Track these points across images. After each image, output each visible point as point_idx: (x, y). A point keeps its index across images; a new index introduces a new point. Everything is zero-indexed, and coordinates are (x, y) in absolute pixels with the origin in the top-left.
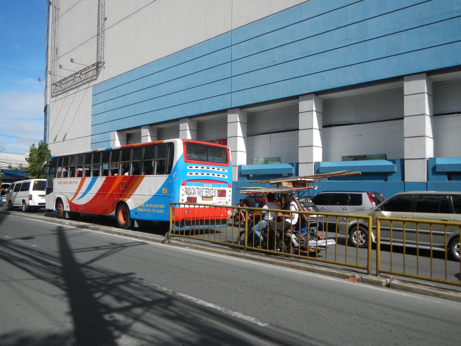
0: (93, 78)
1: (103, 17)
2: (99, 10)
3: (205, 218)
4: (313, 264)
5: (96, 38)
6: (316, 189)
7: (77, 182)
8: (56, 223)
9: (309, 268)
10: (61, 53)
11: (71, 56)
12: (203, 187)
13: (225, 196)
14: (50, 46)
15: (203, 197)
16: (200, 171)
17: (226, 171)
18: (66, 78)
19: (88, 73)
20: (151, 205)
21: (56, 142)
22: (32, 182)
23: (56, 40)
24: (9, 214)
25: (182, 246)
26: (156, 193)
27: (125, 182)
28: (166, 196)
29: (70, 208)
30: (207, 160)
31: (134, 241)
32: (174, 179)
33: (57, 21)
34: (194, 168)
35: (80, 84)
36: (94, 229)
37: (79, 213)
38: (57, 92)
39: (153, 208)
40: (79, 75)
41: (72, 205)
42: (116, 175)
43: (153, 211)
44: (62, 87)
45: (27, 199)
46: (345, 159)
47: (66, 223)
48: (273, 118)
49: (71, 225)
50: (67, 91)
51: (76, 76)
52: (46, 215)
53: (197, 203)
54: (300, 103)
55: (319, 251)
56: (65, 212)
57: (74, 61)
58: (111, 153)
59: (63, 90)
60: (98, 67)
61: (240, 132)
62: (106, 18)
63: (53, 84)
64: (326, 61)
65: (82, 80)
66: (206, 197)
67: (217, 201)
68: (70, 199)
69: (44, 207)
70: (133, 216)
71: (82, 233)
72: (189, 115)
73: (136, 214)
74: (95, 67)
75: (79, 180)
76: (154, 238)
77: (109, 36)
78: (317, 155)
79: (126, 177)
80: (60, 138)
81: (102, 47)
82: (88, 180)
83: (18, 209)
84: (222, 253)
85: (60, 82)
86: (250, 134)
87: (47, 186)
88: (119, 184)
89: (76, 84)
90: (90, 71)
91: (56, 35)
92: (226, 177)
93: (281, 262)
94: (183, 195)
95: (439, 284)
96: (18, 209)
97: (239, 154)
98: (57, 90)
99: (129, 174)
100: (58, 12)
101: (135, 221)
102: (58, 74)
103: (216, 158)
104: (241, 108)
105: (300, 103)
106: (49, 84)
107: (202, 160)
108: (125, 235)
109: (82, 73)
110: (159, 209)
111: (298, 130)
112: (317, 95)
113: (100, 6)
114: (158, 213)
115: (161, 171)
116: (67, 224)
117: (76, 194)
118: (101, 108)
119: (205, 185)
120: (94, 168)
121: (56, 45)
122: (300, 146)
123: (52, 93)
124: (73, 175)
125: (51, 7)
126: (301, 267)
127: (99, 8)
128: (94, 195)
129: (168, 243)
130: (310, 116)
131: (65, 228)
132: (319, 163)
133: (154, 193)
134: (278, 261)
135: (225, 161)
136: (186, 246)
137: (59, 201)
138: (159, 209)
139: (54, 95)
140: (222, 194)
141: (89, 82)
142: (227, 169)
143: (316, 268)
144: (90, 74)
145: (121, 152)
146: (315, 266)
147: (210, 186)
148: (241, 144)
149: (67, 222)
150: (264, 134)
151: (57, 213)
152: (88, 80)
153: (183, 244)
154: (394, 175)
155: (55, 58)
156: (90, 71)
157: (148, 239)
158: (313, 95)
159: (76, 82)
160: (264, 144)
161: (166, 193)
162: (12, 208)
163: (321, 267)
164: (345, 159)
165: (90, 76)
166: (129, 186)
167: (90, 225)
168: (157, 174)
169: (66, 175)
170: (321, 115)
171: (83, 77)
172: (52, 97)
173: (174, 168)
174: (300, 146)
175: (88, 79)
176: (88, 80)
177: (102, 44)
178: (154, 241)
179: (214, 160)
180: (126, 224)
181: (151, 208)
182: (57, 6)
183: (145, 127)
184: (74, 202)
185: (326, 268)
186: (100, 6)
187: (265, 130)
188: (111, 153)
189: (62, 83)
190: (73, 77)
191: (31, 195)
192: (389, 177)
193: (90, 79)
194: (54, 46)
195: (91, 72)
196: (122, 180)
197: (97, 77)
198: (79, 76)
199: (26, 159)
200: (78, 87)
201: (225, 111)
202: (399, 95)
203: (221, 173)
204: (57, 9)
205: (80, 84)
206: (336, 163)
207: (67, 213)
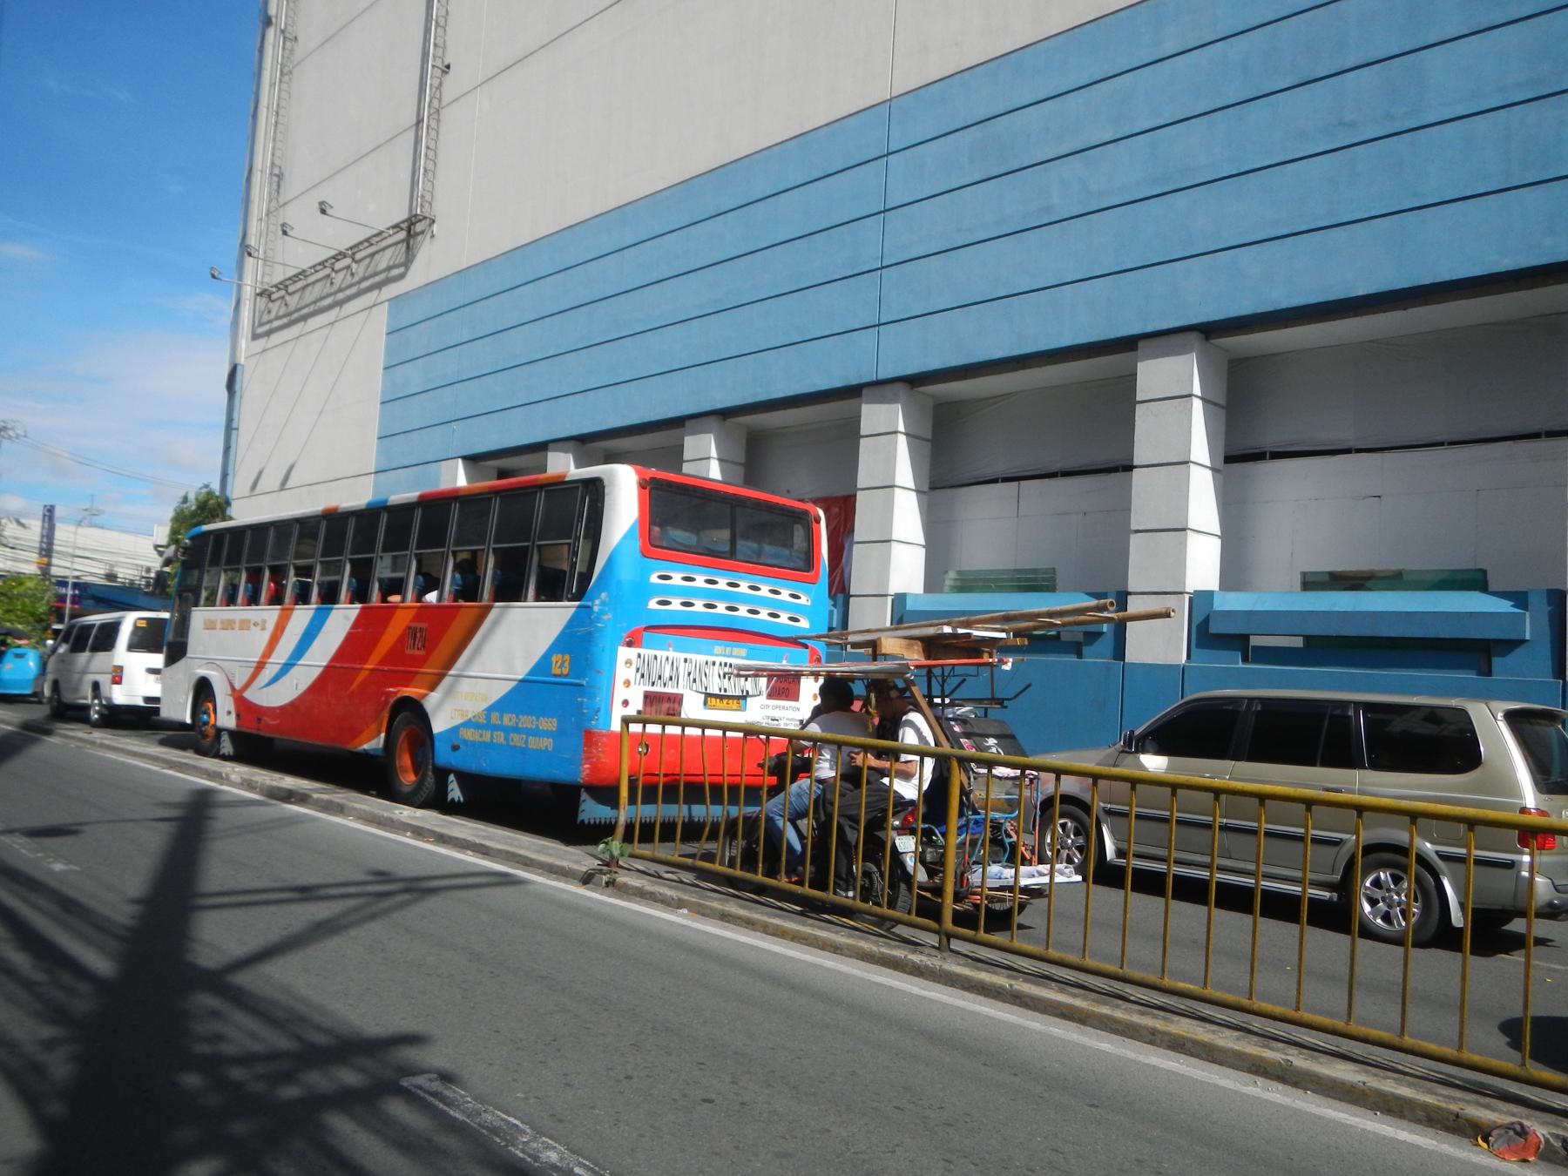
0: (395, 272)
1: (439, 63)
2: (426, 40)
3: (707, 779)
4: (1276, 1039)
5: (411, 135)
6: (1007, 667)
7: (264, 621)
8: (190, 773)
9: (1262, 1059)
10: (292, 187)
11: (326, 194)
12: (710, 659)
13: (795, 698)
14: (258, 164)
15: (708, 695)
16: (699, 593)
17: (803, 601)
18: (303, 273)
19: (377, 257)
20: (508, 720)
21: (258, 490)
22: (129, 621)
23: (279, 145)
24: (49, 733)
25: (666, 903)
26: (531, 673)
27: (424, 625)
28: (566, 680)
29: (238, 716)
30: (732, 554)
31: (477, 870)
32: (598, 619)
33: (286, 79)
34: (677, 579)
35: (349, 292)
36: (327, 807)
37: (271, 740)
38: (270, 322)
39: (516, 729)
40: (347, 261)
41: (244, 707)
42: (395, 599)
43: (517, 740)
44: (290, 305)
45: (104, 680)
46: (1311, 583)
47: (233, 777)
48: (1036, 422)
49: (249, 785)
50: (304, 318)
51: (338, 265)
52: (163, 743)
53: (683, 716)
54: (1140, 365)
55: (1022, 907)
56: (219, 731)
57: (329, 211)
58: (384, 518)
59: (289, 314)
60: (411, 236)
61: (905, 473)
62: (448, 67)
63: (260, 295)
64: (1248, 210)
65: (356, 279)
66: (721, 697)
67: (761, 711)
68: (238, 686)
69: (157, 711)
70: (443, 755)
71: (280, 819)
72: (718, 406)
73: (455, 748)
74: (403, 235)
75: (271, 614)
76: (549, 860)
77: (461, 127)
78: (1202, 565)
79: (430, 607)
80: (270, 481)
81: (430, 166)
82: (302, 616)
83: (78, 714)
84: (836, 949)
85: (283, 285)
86: (942, 479)
87: (170, 636)
88: (404, 633)
89: (335, 293)
90: (384, 249)
91: (280, 127)
92: (804, 623)
93: (1119, 1014)
94: (627, 683)
95: (1391, 1052)
96: (78, 714)
97: (899, 551)
98: (273, 315)
99: (440, 598)
100: (292, 51)
101: (452, 777)
102: (279, 259)
103: (767, 548)
104: (914, 381)
105: (1142, 367)
106: (248, 291)
107: (712, 553)
108: (442, 839)
109: (358, 256)
110: (537, 733)
111: (1129, 468)
112: (1207, 339)
113: (432, 23)
114: (539, 751)
115: (552, 589)
116: (236, 781)
117: (260, 666)
118: (414, 377)
119: (718, 649)
120: (323, 574)
121: (277, 162)
122: (1133, 527)
123: (257, 323)
124: (253, 600)
125: (271, 32)
126: (1222, 1050)
127: (427, 30)
128: (316, 673)
129: (608, 884)
130: (1178, 416)
131: (223, 798)
132: (1209, 595)
133: (521, 670)
134: (1105, 1010)
135: (801, 564)
136: (680, 904)
137: (203, 690)
138: (537, 733)
139: (260, 330)
140: (784, 685)
141: (379, 286)
142: (808, 593)
143: (1300, 1061)
144: (384, 261)
145: (418, 513)
146: (1294, 1051)
147: (739, 655)
148: (906, 516)
149: (237, 771)
150: (995, 481)
151: (193, 737)
152: (377, 279)
153: (669, 892)
154: (1519, 652)
155: (274, 204)
156: (384, 249)
157: (527, 863)
158: (1193, 337)
159: (336, 287)
160: (997, 524)
161: (565, 671)
162: (68, 712)
163: (1323, 1058)
164: (1311, 583)
165: (383, 266)
166: (439, 643)
167: (316, 791)
168: (537, 599)
169: (231, 600)
170: (1222, 413)
171: (359, 269)
172: (255, 337)
173: (600, 577)
174: (1133, 527)
175: (376, 274)
176: (377, 279)
177: (431, 154)
178: (551, 870)
179: (759, 553)
180: (419, 785)
181: (506, 730)
182: (290, 29)
183: (560, 445)
184: (252, 695)
185: (1350, 1066)
186: (432, 23)
187: (999, 468)
188: (384, 518)
189: (291, 289)
190: (328, 271)
191: (120, 668)
192: (1496, 661)
193: (383, 276)
194: (273, 164)
195: (389, 252)
196: (415, 619)
197: (407, 269)
198: (348, 267)
199: (156, 547)
200: (340, 304)
201: (853, 392)
202: (850, 434)
203: (784, 605)
204: (289, 39)
205: (349, 292)
206: (1275, 596)
207: (225, 737)
